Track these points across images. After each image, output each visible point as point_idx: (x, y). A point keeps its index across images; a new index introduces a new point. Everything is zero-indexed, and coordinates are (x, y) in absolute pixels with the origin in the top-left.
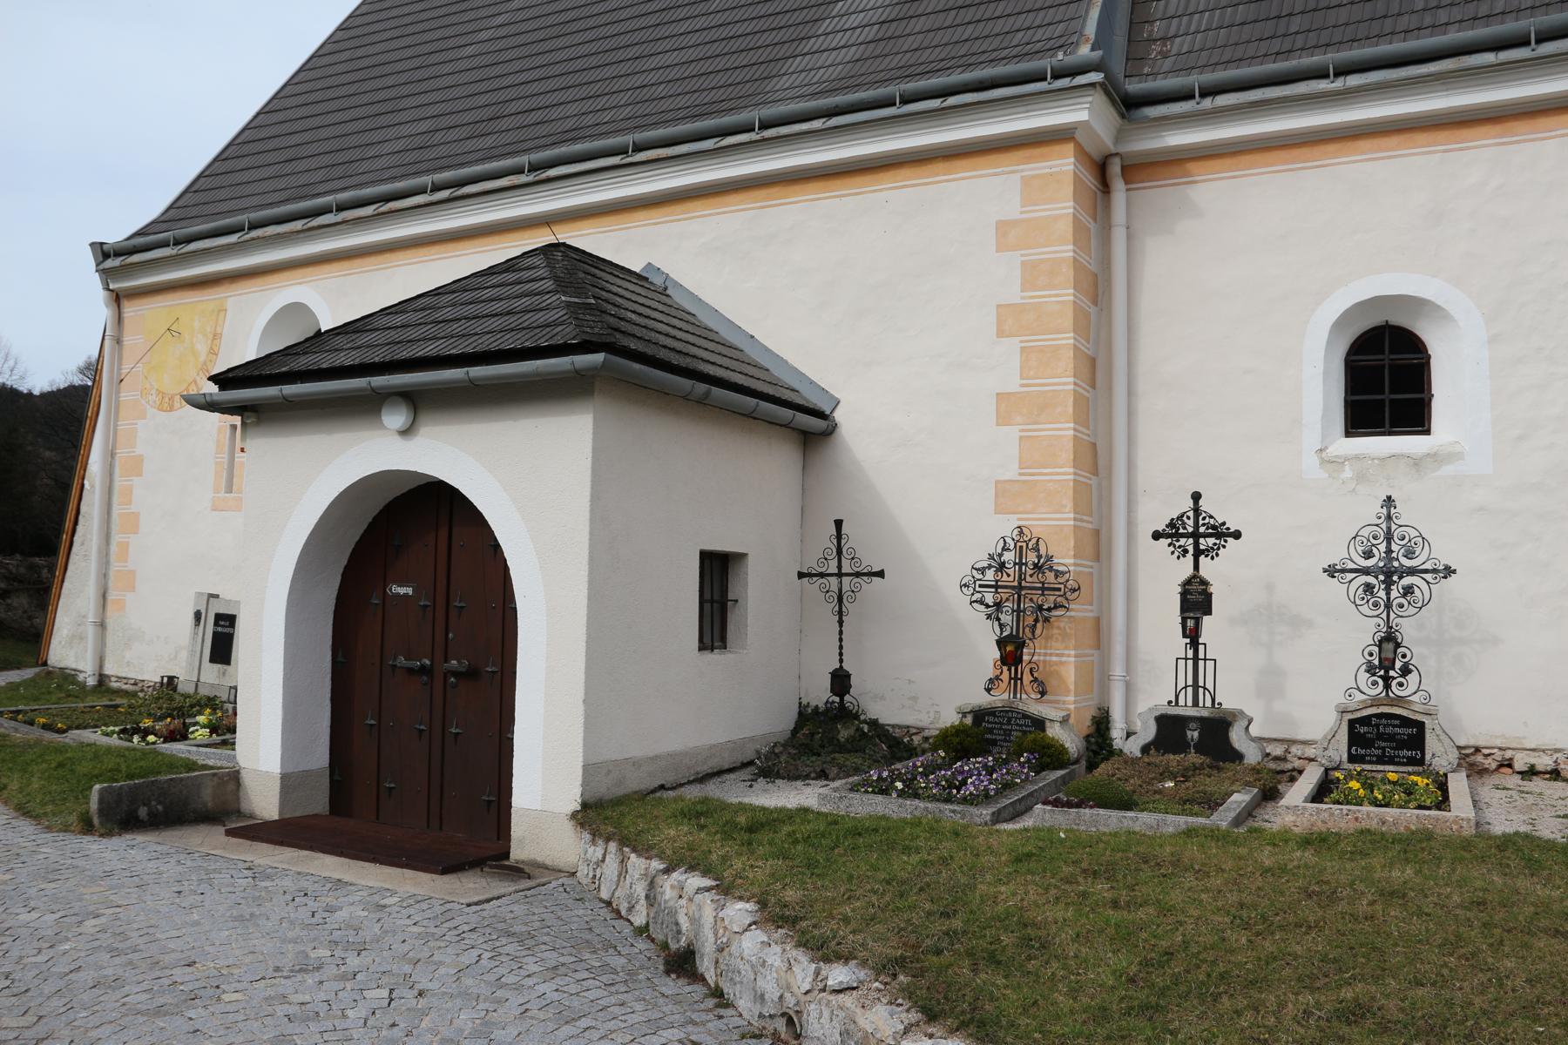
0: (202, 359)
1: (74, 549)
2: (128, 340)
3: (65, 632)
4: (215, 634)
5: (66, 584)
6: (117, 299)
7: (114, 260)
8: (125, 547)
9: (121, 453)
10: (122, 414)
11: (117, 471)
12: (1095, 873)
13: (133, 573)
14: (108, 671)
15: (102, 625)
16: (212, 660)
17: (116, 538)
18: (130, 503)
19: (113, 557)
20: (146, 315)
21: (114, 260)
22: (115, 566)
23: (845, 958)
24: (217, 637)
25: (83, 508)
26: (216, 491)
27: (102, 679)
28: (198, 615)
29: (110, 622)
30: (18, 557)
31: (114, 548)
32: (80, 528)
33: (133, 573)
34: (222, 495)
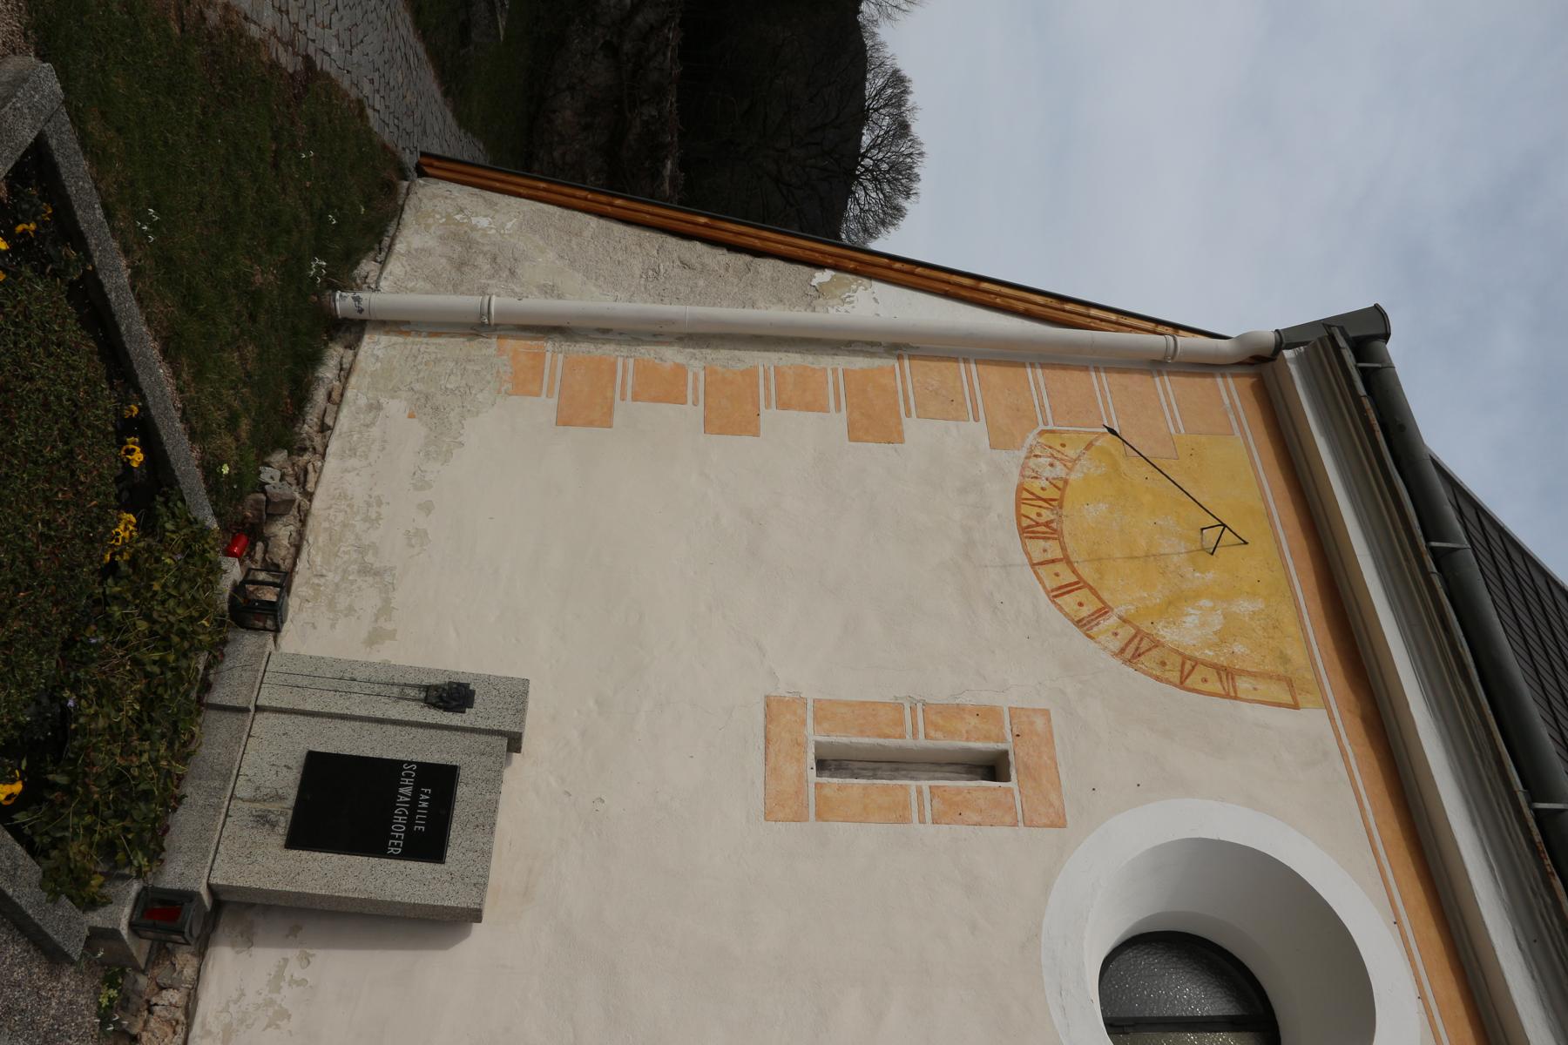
0: (1168, 634)
1: (672, 242)
2: (1166, 387)
3: (483, 222)
4: (393, 768)
5: (593, 222)
6: (1258, 364)
7: (1350, 355)
8: (669, 391)
9: (903, 374)
10: (995, 374)
11: (860, 363)
12: (1226, 673)
13: (606, 421)
14: (374, 347)
15: (479, 327)
16: (315, 762)
17: (695, 363)
18: (784, 405)
19: (648, 353)
20: (1235, 463)
21: (1350, 355)
22: (624, 360)
23: (821, 266)
24: (378, 775)
25: (766, 266)
26: (824, 711)
27: (353, 328)
28: (453, 696)
29: (488, 348)
30: (677, 71)
31: (672, 355)
32: (721, 257)
33: (606, 421)
34: (813, 735)
